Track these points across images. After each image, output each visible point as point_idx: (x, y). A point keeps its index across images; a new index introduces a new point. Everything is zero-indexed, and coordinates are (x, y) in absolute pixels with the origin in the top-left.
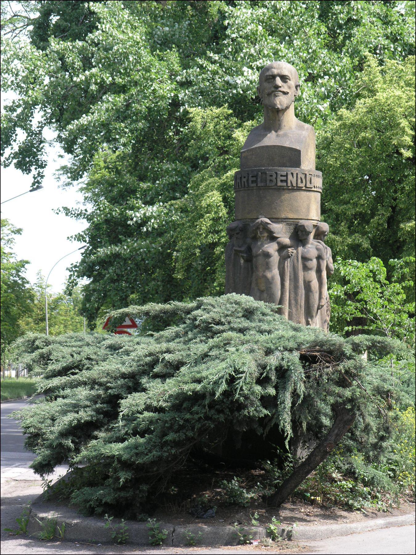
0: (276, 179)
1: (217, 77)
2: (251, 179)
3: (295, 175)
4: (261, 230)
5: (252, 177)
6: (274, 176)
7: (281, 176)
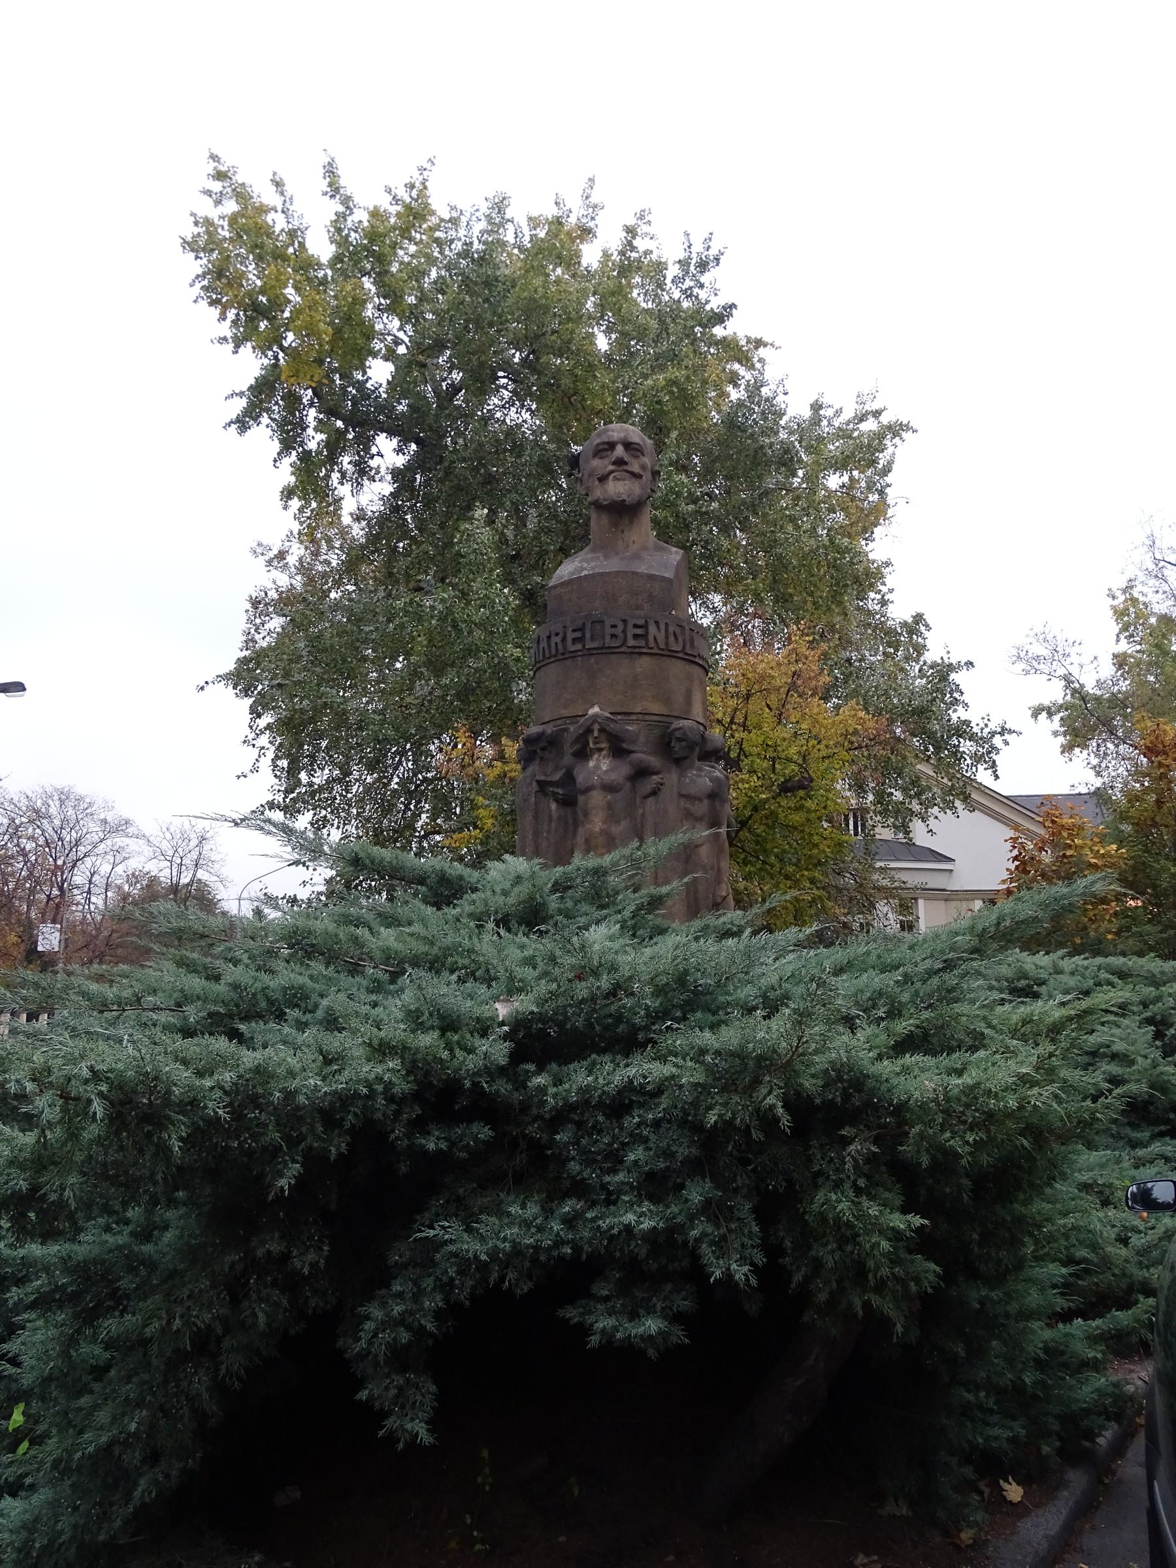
0: (624, 631)
2: (570, 636)
3: (662, 627)
4: (596, 734)
5: (574, 631)
6: (620, 628)
7: (636, 626)
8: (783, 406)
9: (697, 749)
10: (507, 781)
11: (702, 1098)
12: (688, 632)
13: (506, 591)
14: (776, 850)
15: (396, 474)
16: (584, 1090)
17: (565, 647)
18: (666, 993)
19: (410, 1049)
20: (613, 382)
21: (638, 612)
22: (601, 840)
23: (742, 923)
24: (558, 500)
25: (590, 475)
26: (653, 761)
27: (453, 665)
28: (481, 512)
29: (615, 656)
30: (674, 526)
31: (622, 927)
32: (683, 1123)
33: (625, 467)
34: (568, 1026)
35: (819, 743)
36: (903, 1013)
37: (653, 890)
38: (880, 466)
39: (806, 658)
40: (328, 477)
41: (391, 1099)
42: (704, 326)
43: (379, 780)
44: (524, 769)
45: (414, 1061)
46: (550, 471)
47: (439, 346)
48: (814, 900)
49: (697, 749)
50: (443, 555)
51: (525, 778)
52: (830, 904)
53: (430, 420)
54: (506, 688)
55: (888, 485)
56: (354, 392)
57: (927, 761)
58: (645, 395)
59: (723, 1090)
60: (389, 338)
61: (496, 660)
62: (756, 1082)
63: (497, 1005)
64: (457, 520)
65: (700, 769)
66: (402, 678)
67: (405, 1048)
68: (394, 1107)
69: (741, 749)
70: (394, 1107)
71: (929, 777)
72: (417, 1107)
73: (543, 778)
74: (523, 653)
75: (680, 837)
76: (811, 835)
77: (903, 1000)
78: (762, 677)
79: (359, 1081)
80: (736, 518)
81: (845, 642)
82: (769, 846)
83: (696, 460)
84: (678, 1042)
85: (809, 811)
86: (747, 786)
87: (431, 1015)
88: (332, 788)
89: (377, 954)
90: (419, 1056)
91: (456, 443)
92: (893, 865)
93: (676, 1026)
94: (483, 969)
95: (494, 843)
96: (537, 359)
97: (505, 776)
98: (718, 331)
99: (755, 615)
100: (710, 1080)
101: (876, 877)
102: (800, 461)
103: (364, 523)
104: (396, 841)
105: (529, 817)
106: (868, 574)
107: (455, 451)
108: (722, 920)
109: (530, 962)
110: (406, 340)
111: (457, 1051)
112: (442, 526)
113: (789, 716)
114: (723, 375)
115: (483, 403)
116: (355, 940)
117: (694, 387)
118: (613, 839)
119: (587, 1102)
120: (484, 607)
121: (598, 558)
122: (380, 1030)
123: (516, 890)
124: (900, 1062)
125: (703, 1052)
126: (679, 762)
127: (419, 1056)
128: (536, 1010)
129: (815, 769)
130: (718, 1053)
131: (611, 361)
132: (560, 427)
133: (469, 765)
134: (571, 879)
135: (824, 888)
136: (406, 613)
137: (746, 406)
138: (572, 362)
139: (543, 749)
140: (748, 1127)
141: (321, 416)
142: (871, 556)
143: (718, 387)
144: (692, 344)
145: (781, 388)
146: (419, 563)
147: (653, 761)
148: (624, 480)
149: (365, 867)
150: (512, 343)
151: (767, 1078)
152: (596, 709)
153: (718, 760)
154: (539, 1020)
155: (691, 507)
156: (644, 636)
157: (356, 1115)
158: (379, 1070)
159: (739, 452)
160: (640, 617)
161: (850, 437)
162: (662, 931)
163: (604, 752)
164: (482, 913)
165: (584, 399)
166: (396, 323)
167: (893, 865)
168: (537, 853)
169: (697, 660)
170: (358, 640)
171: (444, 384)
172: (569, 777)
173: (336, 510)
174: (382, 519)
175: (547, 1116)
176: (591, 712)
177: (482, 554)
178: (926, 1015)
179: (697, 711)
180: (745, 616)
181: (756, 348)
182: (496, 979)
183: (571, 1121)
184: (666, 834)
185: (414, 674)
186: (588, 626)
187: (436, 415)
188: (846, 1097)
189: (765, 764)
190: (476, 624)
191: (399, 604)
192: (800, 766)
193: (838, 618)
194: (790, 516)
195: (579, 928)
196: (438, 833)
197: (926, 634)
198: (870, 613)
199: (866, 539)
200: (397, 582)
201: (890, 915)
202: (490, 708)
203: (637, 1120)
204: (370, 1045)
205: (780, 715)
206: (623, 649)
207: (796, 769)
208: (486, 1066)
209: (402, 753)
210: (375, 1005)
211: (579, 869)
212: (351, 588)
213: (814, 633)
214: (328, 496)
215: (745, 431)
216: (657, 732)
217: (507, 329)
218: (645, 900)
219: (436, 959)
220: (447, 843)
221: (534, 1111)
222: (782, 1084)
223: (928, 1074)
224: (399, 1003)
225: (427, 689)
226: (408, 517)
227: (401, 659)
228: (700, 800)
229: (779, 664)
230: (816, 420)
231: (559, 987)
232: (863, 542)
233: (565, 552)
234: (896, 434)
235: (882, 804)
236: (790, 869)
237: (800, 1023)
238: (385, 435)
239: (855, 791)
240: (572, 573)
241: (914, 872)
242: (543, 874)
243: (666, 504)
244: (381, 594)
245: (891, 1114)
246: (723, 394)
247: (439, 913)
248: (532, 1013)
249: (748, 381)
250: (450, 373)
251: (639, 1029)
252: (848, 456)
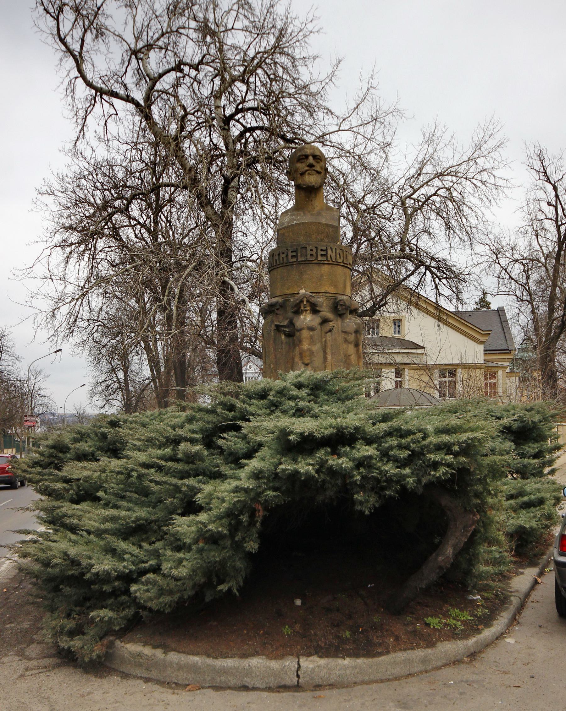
0: (317, 253)
2: (290, 254)
3: (334, 250)
6: (315, 251)
7: (322, 250)
26: (330, 315)
29: (311, 265)
65: (350, 319)
73: (278, 323)
139: (278, 309)
156: (326, 255)
172: (291, 323)
216: (332, 301)
240: (288, 222)
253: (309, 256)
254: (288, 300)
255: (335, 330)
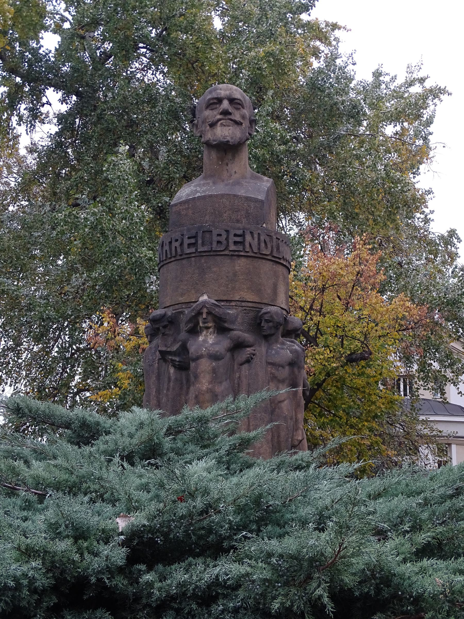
0: (227, 239)
1: (374, 325)
2: (186, 242)
3: (256, 236)
4: (204, 316)
5: (189, 238)
6: (224, 236)
7: (235, 235)
8: (352, 73)
9: (281, 328)
10: (140, 351)
11: (269, 590)
12: (275, 240)
13: (143, 207)
14: (343, 406)
15: (61, 118)
16: (181, 585)
17: (182, 250)
18: (246, 511)
19: (50, 552)
20: (226, 53)
21: (239, 225)
22: (207, 396)
23: (310, 460)
24: (183, 140)
25: (203, 122)
26: (248, 337)
27: (101, 262)
28: (124, 148)
29: (219, 258)
30: (270, 161)
31: (219, 462)
32: (256, 610)
33: (230, 117)
34: (171, 536)
35: (377, 325)
36: (423, 527)
37: (244, 434)
38: (425, 119)
39: (367, 261)
40: (9, 119)
41: (34, 591)
42: (294, 13)
43: (43, 349)
44: (150, 342)
45: (53, 562)
46: (177, 118)
47: (95, 23)
48: (372, 444)
49: (281, 328)
50: (95, 179)
51: (150, 348)
52: (383, 447)
53: (87, 79)
54: (141, 280)
55: (431, 134)
56: (30, 56)
57: (458, 340)
58: (249, 63)
59: (286, 584)
60: (57, 17)
61: (134, 260)
62: (309, 578)
63: (118, 520)
64: (106, 153)
65: (283, 344)
66: (62, 272)
67: (46, 552)
68: (36, 597)
69: (318, 329)
70: (36, 597)
71: (459, 352)
72: (54, 597)
73: (164, 349)
74: (154, 255)
75: (264, 394)
76: (370, 395)
77: (423, 518)
78: (334, 275)
79: (8, 577)
80: (317, 156)
81: (398, 250)
82: (338, 403)
83: (287, 112)
84: (253, 548)
85: (368, 377)
86: (322, 357)
87: (67, 526)
88: (7, 355)
89: (30, 481)
90: (57, 558)
91: (106, 96)
92: (432, 418)
93: (249, 535)
94: (109, 492)
95: (130, 398)
96: (169, 34)
97: (139, 347)
98: (304, 17)
99: (330, 229)
100: (275, 577)
101: (419, 427)
102: (365, 114)
103: (36, 155)
104: (55, 396)
105: (154, 378)
106: (414, 199)
107: (105, 102)
108: (295, 457)
109: (145, 488)
110: (70, 18)
111: (86, 555)
112: (95, 158)
113: (353, 306)
114: (307, 50)
115: (126, 67)
116: (13, 470)
117: (285, 58)
118: (216, 396)
119: (184, 594)
120: (125, 219)
121: (208, 184)
122: (27, 538)
123: (139, 433)
124: (419, 564)
125: (270, 555)
126: (266, 338)
127: (57, 558)
128: (147, 523)
129: (373, 344)
130: (281, 556)
131: (224, 37)
132: (185, 85)
133: (112, 339)
134: (181, 425)
135: (380, 435)
136: (66, 222)
137: (324, 73)
138: (195, 38)
139: (165, 327)
140: (303, 613)
141: (5, 74)
142: (417, 186)
143: (303, 58)
144: (285, 26)
145: (351, 60)
146: (77, 185)
147: (248, 337)
148: (229, 126)
149: (24, 415)
150: (150, 22)
151: (317, 575)
152: (205, 297)
153: (297, 336)
154: (149, 532)
155: (283, 147)
157: (6, 602)
158: (25, 568)
159: (319, 107)
160: (239, 229)
161: (402, 97)
162: (250, 466)
163: (211, 330)
164: (113, 451)
165: (203, 65)
166: (63, 6)
167: (432, 418)
168: (159, 406)
169: (282, 261)
170: (29, 243)
171: (98, 52)
172: (184, 348)
173: (15, 144)
174: (50, 152)
175: (154, 605)
176: (201, 299)
177: (124, 180)
178: (440, 529)
179: (282, 300)
180: (323, 229)
181: (333, 30)
182: (119, 500)
183: (172, 608)
184: (256, 390)
185: (72, 269)
186: (200, 235)
187: (92, 75)
188: (378, 590)
189: (336, 341)
190: (119, 232)
191: (60, 216)
192: (362, 343)
193: (392, 232)
194: (356, 155)
195: (186, 462)
196: (88, 390)
197: (458, 245)
198: (416, 229)
199: (414, 173)
200: (60, 199)
201: (430, 456)
202: (128, 296)
203: (221, 607)
204: (19, 549)
205: (348, 303)
206: (226, 252)
207: (359, 345)
208: (108, 567)
209: (62, 329)
210: (25, 519)
211: (187, 418)
212: (25, 203)
213: (374, 243)
214: (8, 133)
215: (323, 91)
216: (252, 315)
217: (146, 12)
218: (237, 442)
219: (74, 485)
220: (94, 398)
221: (144, 601)
222: (328, 580)
223: (440, 573)
224: (43, 517)
225: (81, 281)
226: (70, 150)
227: (61, 258)
228: (283, 367)
229: (347, 266)
230: (377, 84)
231: (165, 506)
232: (412, 176)
233: (187, 178)
234: (436, 96)
235: (424, 372)
236: (354, 420)
237: (341, 533)
238: (53, 88)
239: (404, 362)
240: (188, 195)
241: (449, 424)
242: (160, 421)
243: (264, 144)
244: (48, 208)
245: (412, 604)
246: (308, 64)
247: (80, 450)
248: (144, 526)
249: (326, 55)
250: (103, 43)
251: (224, 539)
252: (400, 112)
253: (215, 244)
254: (181, 313)
255: (256, 360)
